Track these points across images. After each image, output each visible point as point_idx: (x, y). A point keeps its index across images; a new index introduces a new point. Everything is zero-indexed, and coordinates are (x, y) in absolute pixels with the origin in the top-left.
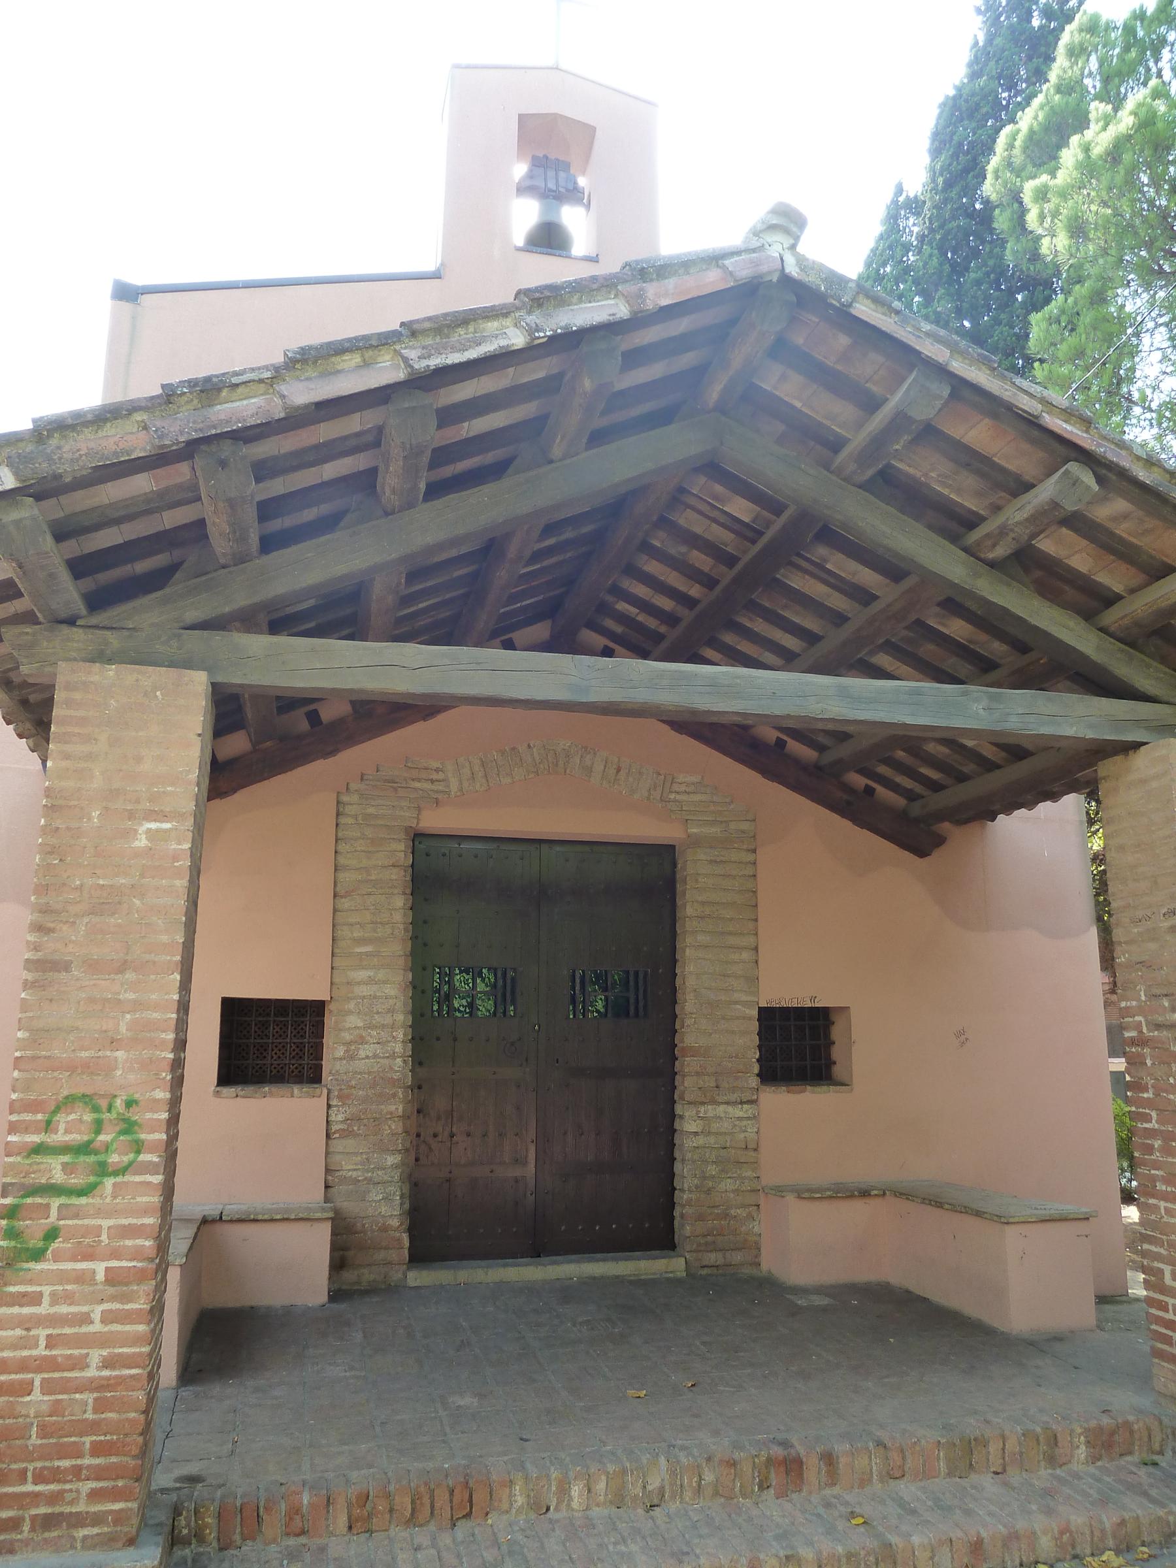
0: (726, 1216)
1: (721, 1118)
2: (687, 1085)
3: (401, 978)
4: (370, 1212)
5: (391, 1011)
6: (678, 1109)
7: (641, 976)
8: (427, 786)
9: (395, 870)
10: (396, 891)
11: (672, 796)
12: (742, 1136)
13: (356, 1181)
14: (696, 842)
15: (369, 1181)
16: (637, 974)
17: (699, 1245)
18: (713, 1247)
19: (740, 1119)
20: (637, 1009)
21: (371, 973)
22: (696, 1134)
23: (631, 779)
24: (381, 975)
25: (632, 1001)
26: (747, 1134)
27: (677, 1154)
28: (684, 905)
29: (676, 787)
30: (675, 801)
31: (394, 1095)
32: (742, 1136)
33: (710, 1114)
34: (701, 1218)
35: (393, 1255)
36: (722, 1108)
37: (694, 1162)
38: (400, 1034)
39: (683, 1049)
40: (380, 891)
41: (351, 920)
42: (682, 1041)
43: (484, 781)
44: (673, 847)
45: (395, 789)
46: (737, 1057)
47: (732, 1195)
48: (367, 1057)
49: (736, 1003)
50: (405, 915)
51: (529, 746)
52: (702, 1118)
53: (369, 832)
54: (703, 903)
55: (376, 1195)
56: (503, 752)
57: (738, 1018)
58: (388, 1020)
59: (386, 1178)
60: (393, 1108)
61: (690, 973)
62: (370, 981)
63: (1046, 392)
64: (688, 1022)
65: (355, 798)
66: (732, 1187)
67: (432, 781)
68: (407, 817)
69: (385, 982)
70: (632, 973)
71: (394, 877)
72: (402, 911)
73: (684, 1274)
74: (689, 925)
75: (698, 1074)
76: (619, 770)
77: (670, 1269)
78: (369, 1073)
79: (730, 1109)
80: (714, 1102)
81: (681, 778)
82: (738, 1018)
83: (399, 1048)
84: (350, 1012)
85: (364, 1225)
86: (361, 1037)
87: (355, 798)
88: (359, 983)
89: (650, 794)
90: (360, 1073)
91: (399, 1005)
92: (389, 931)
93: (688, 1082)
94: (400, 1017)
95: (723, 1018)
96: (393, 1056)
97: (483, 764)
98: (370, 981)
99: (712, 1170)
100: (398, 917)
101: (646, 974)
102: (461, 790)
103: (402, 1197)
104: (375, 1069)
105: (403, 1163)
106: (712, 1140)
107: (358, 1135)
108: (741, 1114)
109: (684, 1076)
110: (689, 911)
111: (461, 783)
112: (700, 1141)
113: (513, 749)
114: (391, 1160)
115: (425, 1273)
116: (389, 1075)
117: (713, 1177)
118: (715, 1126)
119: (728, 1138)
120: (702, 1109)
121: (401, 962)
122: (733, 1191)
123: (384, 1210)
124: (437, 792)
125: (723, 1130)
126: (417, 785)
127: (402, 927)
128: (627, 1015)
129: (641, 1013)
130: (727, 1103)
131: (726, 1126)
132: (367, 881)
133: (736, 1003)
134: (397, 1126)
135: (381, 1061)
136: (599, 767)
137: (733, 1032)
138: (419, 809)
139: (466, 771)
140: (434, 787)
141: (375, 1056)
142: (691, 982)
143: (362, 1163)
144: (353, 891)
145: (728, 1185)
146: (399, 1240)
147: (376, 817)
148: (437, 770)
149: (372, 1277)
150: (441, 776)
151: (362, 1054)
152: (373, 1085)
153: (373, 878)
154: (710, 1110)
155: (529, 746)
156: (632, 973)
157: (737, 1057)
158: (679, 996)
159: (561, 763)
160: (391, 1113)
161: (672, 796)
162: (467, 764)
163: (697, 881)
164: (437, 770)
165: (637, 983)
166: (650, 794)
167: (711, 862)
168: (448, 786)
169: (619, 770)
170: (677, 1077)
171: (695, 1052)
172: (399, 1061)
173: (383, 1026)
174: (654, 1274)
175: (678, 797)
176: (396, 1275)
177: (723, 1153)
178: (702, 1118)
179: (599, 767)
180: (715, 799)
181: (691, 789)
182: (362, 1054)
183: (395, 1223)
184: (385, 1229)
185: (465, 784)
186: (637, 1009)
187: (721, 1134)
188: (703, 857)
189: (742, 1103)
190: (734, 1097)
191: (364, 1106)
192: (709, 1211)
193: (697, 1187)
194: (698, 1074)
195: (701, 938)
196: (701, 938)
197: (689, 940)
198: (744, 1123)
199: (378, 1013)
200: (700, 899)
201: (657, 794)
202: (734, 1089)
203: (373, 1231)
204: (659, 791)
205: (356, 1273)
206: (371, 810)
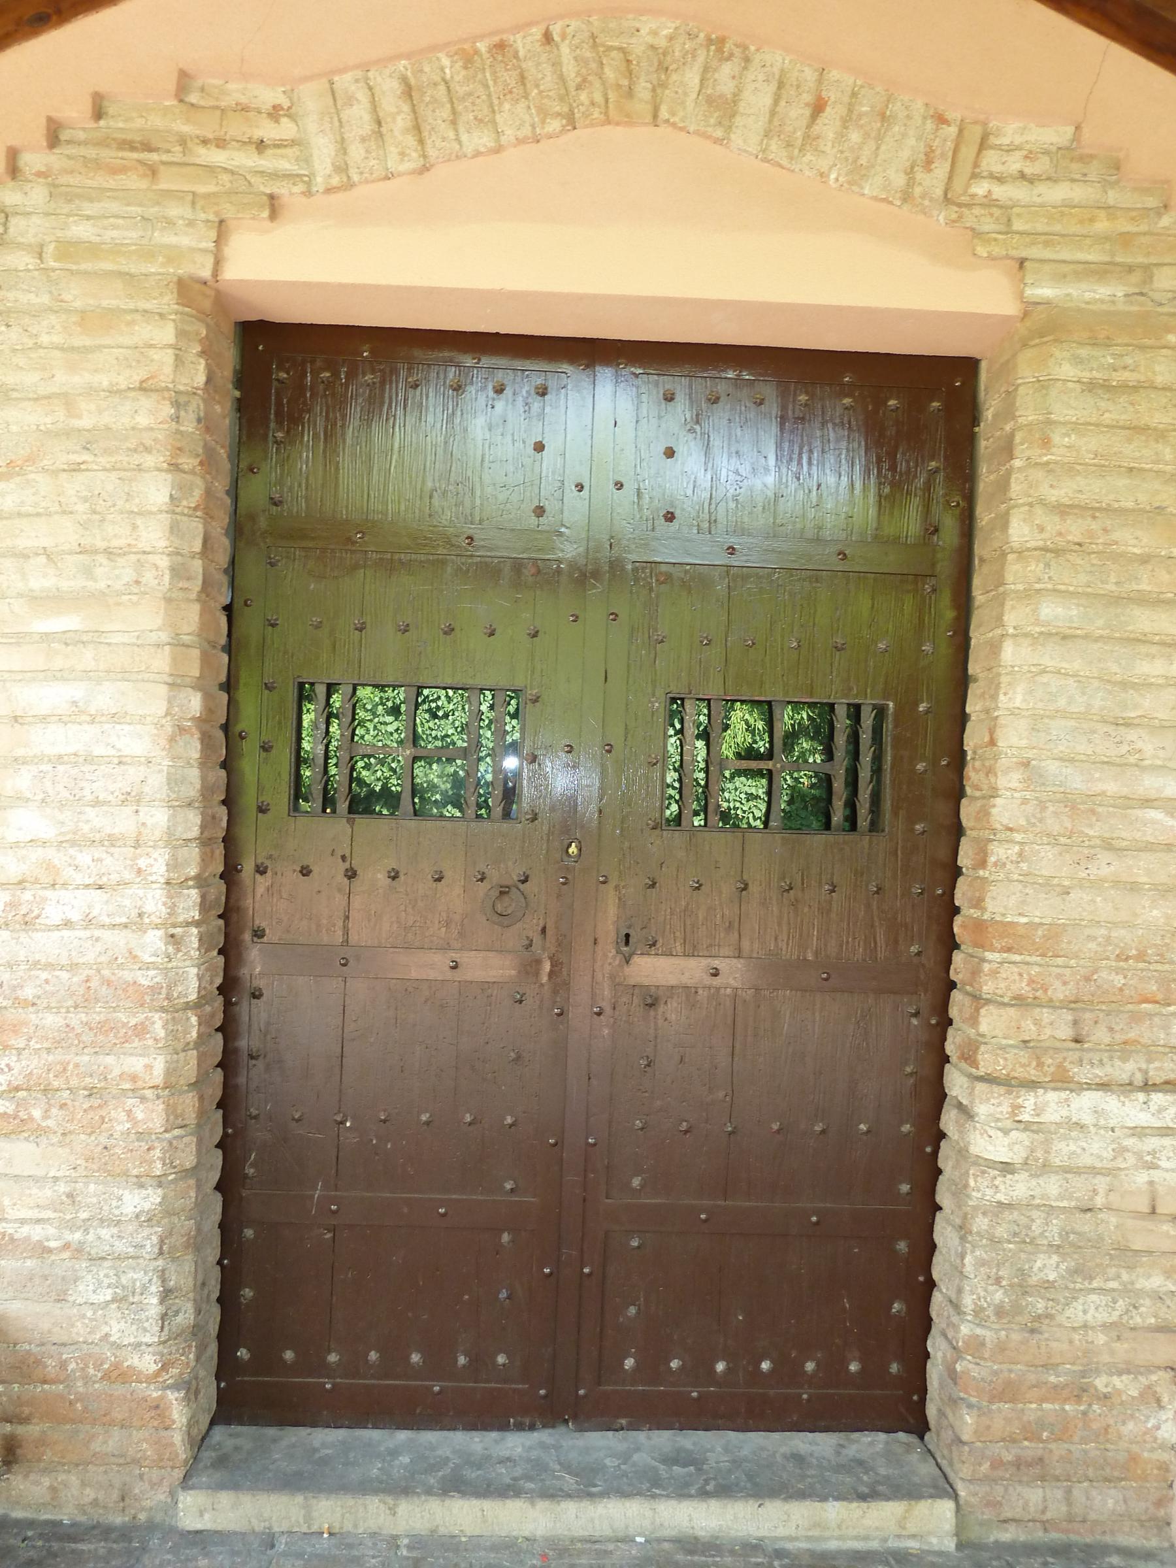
0: (1080, 1391)
1: (1081, 1127)
2: (992, 1024)
3: (160, 707)
4: (79, 1331)
5: (133, 799)
6: (956, 1082)
7: (867, 720)
8: (246, 160)
9: (146, 402)
10: (150, 460)
11: (980, 189)
12: (1142, 1178)
13: (42, 1250)
14: (1045, 326)
15: (78, 1251)
16: (855, 712)
17: (997, 1464)
18: (1034, 1469)
19: (1139, 1132)
20: (851, 805)
21: (76, 691)
22: (1006, 1168)
23: (855, 137)
24: (105, 698)
25: (838, 785)
26: (1156, 1175)
27: (943, 1196)
28: (1003, 522)
29: (992, 161)
30: (989, 202)
31: (141, 1030)
32: (1142, 1178)
33: (1052, 1115)
34: (1008, 1392)
35: (141, 1442)
36: (1089, 1099)
37: (994, 1241)
38: (157, 863)
39: (979, 926)
40: (103, 460)
41: (22, 543)
42: (978, 903)
43: (411, 141)
44: (967, 367)
45: (153, 171)
46: (1141, 957)
47: (1101, 1339)
48: (68, 924)
49: (1147, 802)
50: (174, 529)
51: (548, 38)
52: (1027, 1127)
53: (76, 295)
54: (1062, 510)
55: (93, 1289)
56: (468, 59)
57: (1149, 847)
58: (124, 823)
59: (121, 1247)
60: (136, 1064)
61: (1014, 713)
62: (77, 714)
63: (173, 1523)
64: (998, 852)
65: (37, 195)
66: (1103, 1316)
67: (261, 145)
68: (188, 244)
69: (116, 718)
70: (841, 711)
71: (143, 420)
72: (165, 518)
73: (950, 1545)
74: (1016, 574)
75: (1019, 1001)
76: (818, 108)
77: (912, 1528)
78: (73, 967)
79: (1111, 1103)
80: (1062, 1081)
81: (1010, 132)
82: (1149, 847)
83: (155, 902)
84: (20, 799)
85: (63, 1365)
86: (49, 866)
87: (37, 195)
88: (44, 719)
89: (911, 182)
90: (49, 966)
91: (156, 782)
92: (128, 575)
93: (991, 1022)
94: (158, 818)
95: (1108, 845)
96: (138, 923)
97: (408, 91)
98: (77, 714)
99: (1047, 1267)
100: (154, 536)
101: (880, 712)
102: (342, 168)
103: (166, 1294)
104: (90, 957)
105: (167, 1210)
106: (1052, 1186)
107: (46, 1131)
108: (1144, 1119)
109: (978, 1000)
110: (1019, 531)
111: (342, 146)
112: (1019, 1187)
113: (501, 46)
114: (139, 1201)
115: (225, 1498)
116: (128, 976)
117: (1048, 1285)
118: (1063, 1150)
119: (1101, 1183)
120: (1029, 1100)
121: (162, 662)
122: (1105, 1327)
123: (118, 1328)
124: (275, 176)
125: (1087, 1160)
126: (217, 157)
127: (164, 562)
128: (827, 826)
129: (863, 822)
130: (1104, 1086)
131: (1096, 1149)
132: (68, 433)
133: (1147, 802)
134: (151, 1115)
135: (106, 935)
136: (757, 100)
137: (1134, 887)
138: (222, 229)
139: (358, 116)
140: (267, 162)
141: (89, 922)
142: (1013, 738)
143: (54, 1206)
144: (30, 459)
145: (1091, 1308)
146: (157, 1407)
147: (93, 250)
148: (275, 113)
149: (90, 1494)
150: (286, 129)
151: (53, 914)
152: (87, 1001)
153: (86, 422)
154: (1052, 1105)
155: (548, 38)
156: (841, 711)
157: (1141, 957)
158: (973, 775)
159: (643, 89)
160: (134, 1078)
161: (980, 189)
162: (362, 96)
163: (1046, 443)
164: (275, 113)
165: (854, 738)
166: (911, 182)
167: (1091, 387)
168: (308, 161)
169: (818, 108)
170: (956, 995)
171: (1015, 939)
172: (155, 940)
173: (112, 841)
174: (866, 1538)
175: (1000, 192)
176: (150, 1498)
177: (1084, 1224)
178: (1027, 1127)
179: (757, 100)
180: (1112, 197)
181: (1042, 166)
182: (53, 914)
183: (147, 1363)
184: (120, 1375)
185: (356, 152)
186: (851, 805)
187: (1078, 1171)
188: (1067, 371)
189: (1148, 1087)
190: (1124, 1070)
191: (57, 1056)
192: (1032, 1378)
193: (1000, 1312)
194: (1019, 1001)
195: (1051, 611)
196: (1051, 611)
197: (1013, 617)
198: (1153, 1143)
199: (97, 803)
200: (1054, 496)
201: (933, 181)
202: (1125, 1049)
203: (87, 1380)
204: (941, 170)
205: (46, 1481)
206: (82, 231)
